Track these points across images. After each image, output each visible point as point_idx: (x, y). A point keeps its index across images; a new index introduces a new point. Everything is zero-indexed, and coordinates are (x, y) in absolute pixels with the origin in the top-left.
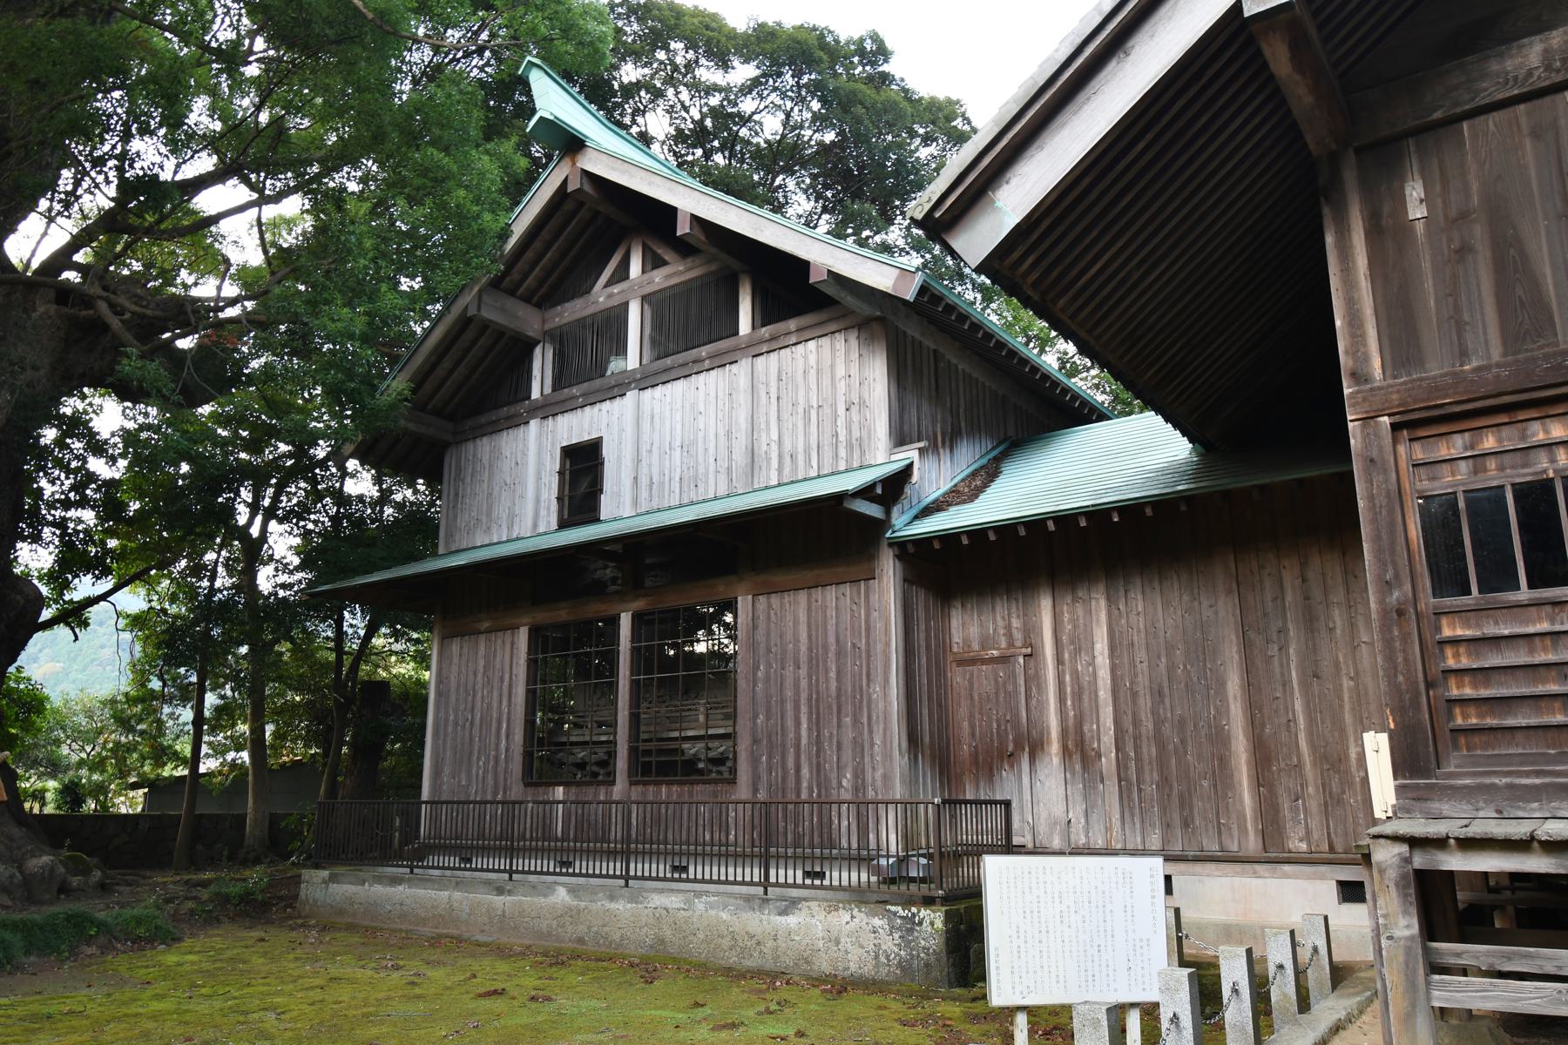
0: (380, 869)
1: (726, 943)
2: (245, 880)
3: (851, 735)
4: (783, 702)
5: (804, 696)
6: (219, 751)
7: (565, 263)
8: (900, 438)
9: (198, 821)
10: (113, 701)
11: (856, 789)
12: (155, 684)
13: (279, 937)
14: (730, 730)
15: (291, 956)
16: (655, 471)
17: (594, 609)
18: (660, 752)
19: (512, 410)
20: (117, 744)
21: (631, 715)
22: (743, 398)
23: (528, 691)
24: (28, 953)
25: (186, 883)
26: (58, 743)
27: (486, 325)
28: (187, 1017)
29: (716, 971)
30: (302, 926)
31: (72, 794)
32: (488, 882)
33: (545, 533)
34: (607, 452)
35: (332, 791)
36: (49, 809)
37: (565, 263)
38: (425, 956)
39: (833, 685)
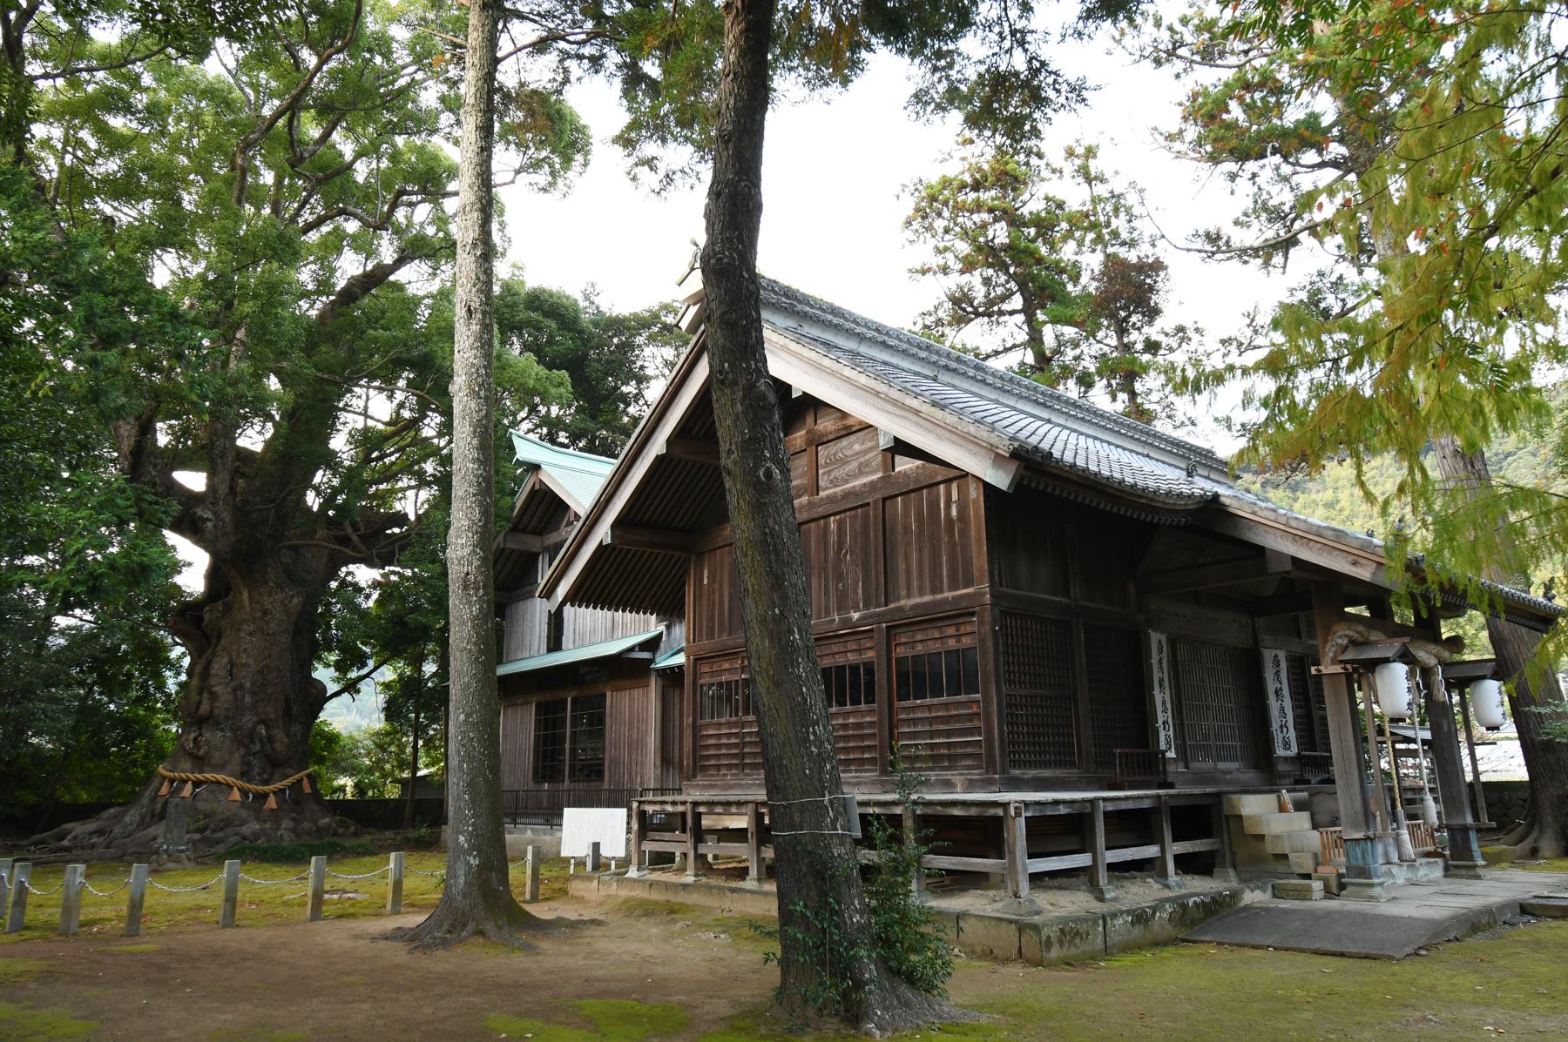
36: (349, 796)
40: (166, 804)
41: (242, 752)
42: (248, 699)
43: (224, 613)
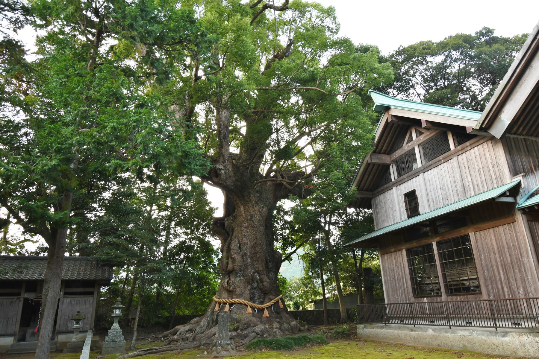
1: (486, 346)
3: (519, 276)
4: (492, 266)
5: (499, 264)
8: (515, 172)
9: (328, 311)
10: (301, 279)
11: (525, 294)
12: (310, 274)
13: (353, 343)
14: (476, 277)
16: (434, 197)
17: (425, 242)
18: (454, 285)
19: (387, 185)
20: (305, 291)
21: (443, 274)
22: (457, 170)
23: (409, 269)
24: (296, 345)
26: (290, 291)
27: (374, 164)
29: (484, 355)
31: (296, 305)
32: (408, 328)
33: (404, 221)
34: (418, 193)
39: (509, 259)
40: (218, 316)
41: (249, 287)
42: (249, 260)
43: (233, 221)
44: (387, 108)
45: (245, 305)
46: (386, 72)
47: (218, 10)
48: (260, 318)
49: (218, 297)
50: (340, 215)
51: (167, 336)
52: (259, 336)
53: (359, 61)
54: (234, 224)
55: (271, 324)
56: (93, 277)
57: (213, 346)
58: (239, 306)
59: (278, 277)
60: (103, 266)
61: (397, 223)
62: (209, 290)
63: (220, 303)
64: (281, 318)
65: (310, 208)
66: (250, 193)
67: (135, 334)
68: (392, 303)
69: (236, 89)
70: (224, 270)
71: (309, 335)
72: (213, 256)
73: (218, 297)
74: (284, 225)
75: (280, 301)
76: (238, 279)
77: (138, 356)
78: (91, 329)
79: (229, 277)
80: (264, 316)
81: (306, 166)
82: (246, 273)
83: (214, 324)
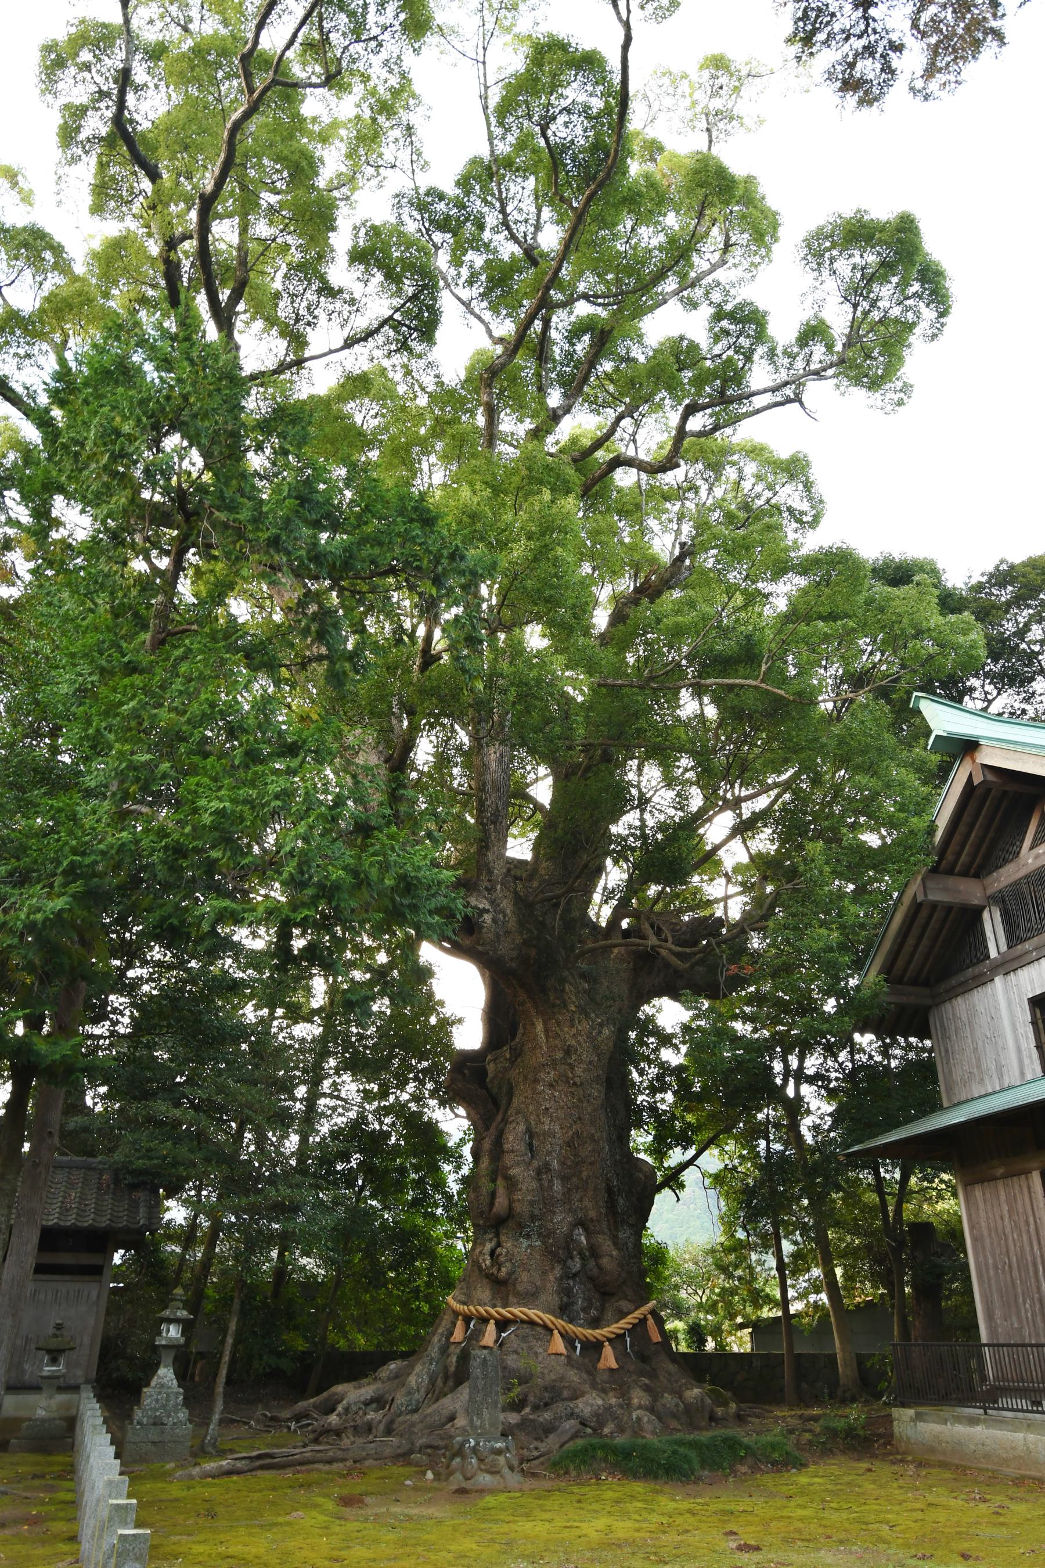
0: (959, 1410)
2: (846, 1417)
6: (803, 1296)
7: (991, 834)
9: (798, 1359)
10: (713, 1251)
12: (741, 1235)
13: (884, 1470)
15: (895, 1485)
20: (723, 1289)
24: (703, 1468)
25: (801, 1417)
26: (677, 1287)
27: (934, 906)
28: (824, 1522)
30: (901, 1461)
31: (696, 1333)
35: (905, 1334)
37: (991, 834)
38: (1010, 1493)
41: (558, 1271)
42: (557, 1186)
43: (512, 1061)
44: (969, 746)
45: (545, 1327)
46: (961, 639)
47: (489, 479)
48: (589, 1373)
49: (463, 1298)
50: (831, 1051)
51: (307, 1416)
52: (589, 1431)
53: (882, 610)
54: (513, 1074)
55: (624, 1393)
56: (104, 1222)
57: (454, 1456)
58: (526, 1329)
59: (644, 1241)
60: (134, 1187)
61: (1010, 1088)
62: (430, 1275)
63: (467, 1319)
64: (653, 1375)
65: (738, 1026)
66: (562, 981)
67: (219, 1405)
68: (1002, 1341)
69: (531, 690)
70: (482, 1213)
71: (746, 1436)
72: (447, 1168)
73: (463, 1298)
74: (659, 1077)
75: (651, 1322)
76: (525, 1243)
77: (229, 1473)
78: (87, 1381)
79: (497, 1235)
80: (601, 1365)
81: (726, 898)
82: (550, 1226)
83: (451, 1383)
